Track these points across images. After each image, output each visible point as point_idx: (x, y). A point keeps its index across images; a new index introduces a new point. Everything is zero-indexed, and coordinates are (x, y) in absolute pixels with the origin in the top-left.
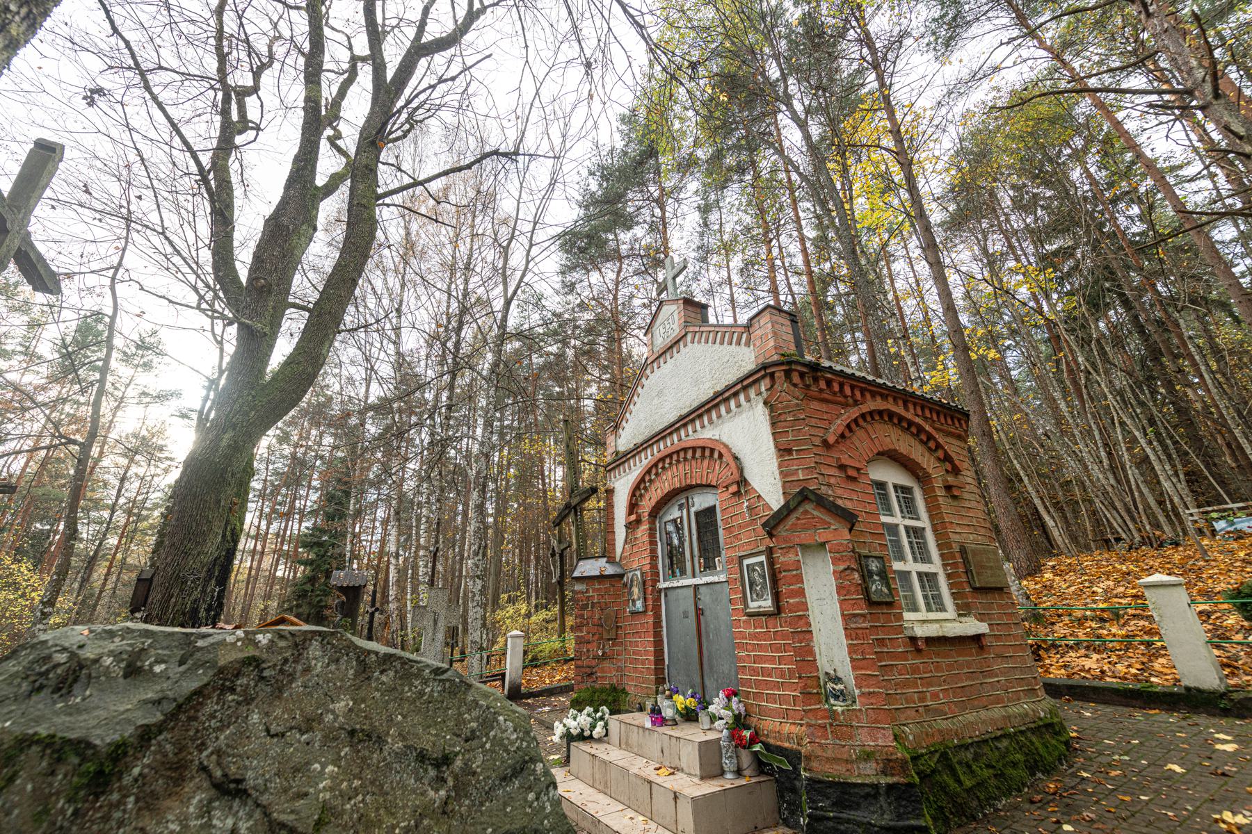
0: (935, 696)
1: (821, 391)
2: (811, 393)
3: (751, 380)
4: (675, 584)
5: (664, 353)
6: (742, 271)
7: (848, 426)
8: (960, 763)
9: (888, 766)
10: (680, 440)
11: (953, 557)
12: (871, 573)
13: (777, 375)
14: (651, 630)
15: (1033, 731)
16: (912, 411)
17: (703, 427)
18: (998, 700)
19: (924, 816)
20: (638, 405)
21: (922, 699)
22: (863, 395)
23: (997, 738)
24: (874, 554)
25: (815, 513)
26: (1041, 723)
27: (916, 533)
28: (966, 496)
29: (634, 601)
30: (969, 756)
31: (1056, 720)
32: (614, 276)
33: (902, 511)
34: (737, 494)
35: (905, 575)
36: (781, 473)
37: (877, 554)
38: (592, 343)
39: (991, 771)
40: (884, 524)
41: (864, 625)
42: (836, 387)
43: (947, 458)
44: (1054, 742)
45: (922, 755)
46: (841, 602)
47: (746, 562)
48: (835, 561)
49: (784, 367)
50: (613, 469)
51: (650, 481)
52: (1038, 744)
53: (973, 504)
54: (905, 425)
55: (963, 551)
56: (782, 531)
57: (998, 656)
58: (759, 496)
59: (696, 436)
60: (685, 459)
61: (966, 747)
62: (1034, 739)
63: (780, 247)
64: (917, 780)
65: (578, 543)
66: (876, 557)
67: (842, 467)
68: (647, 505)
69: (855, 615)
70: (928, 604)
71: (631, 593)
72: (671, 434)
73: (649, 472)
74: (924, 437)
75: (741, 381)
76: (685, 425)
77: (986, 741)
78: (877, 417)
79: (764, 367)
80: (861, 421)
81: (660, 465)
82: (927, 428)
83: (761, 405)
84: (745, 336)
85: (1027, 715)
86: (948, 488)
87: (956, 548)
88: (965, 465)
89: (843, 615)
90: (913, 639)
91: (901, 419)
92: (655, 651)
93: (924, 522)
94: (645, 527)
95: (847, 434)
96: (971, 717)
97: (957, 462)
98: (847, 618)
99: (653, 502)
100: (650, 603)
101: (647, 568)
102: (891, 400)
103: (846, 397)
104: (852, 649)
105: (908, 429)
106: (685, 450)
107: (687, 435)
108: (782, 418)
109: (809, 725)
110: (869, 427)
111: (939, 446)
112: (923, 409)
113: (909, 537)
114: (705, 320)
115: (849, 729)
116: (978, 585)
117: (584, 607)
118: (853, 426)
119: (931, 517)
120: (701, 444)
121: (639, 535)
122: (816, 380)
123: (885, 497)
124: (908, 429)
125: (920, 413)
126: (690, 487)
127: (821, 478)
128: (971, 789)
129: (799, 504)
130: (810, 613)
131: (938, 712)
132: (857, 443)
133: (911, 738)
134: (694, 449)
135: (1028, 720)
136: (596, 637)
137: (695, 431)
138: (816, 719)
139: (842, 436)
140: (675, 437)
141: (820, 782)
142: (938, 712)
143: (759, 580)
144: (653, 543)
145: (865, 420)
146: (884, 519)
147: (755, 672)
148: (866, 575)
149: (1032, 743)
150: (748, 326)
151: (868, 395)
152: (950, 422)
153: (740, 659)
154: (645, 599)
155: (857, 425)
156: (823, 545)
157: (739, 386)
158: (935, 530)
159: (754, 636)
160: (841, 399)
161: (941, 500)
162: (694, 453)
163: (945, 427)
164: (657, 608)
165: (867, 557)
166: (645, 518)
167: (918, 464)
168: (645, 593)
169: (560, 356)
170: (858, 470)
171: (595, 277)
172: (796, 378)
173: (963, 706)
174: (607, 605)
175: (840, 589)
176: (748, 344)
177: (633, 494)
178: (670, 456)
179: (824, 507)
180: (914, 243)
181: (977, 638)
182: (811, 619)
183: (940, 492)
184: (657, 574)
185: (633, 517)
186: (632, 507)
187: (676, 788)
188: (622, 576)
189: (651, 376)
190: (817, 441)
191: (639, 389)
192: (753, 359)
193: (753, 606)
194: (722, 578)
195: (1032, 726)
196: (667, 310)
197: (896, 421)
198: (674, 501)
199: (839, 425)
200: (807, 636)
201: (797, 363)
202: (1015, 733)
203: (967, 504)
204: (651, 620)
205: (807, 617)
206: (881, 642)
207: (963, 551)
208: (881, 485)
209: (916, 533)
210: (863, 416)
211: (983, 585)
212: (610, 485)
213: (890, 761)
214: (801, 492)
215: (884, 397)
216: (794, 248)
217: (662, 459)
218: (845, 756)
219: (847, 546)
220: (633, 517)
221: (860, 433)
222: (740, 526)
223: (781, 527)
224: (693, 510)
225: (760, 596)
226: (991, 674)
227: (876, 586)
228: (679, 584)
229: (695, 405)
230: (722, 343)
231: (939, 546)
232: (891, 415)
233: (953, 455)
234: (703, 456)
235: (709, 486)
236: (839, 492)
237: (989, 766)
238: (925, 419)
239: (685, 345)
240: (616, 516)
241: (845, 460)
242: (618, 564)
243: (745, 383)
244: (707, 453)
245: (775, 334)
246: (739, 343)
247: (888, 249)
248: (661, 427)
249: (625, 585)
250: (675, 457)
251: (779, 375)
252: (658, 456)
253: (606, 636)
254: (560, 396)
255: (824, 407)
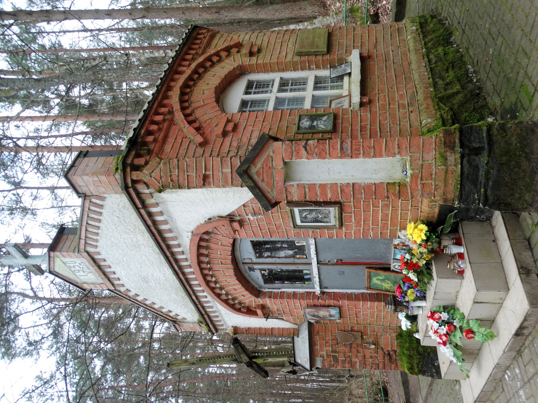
0: (401, 97)
1: (155, 140)
2: (156, 150)
3: (137, 201)
4: (317, 280)
5: (104, 274)
6: (43, 175)
7: (190, 123)
8: (446, 90)
9: (449, 145)
10: (190, 266)
11: (304, 62)
12: (312, 127)
13: (135, 178)
14: (354, 302)
15: (424, 37)
16: (184, 69)
17: (179, 246)
18: (405, 54)
19: (480, 126)
20: (155, 301)
21: (404, 107)
22: (164, 106)
23: (429, 61)
24: (297, 122)
25: (259, 165)
26: (420, 30)
27: (284, 85)
28: (259, 42)
29: (330, 316)
30: (440, 82)
31: (418, 20)
32: (28, 301)
33: (266, 92)
34: (241, 223)
35: (315, 99)
36: (224, 186)
37: (297, 119)
38: (98, 324)
39: (450, 70)
40: (275, 109)
41: (349, 143)
42: (154, 127)
43: (228, 49)
44: (432, 25)
45: (441, 115)
46: (331, 156)
47: (299, 222)
48: (299, 157)
49: (128, 169)
50: (214, 326)
51: (227, 294)
52: (433, 36)
53: (266, 39)
54: (196, 76)
55: (300, 54)
56: (273, 195)
57: (376, 47)
58: (244, 206)
59: (187, 251)
60: (208, 263)
61: (435, 85)
62: (430, 37)
63: (28, 138)
64: (456, 125)
65: (283, 356)
66: (300, 120)
67: (225, 134)
68: (249, 299)
69: (342, 148)
70: (337, 87)
71: (324, 318)
72: (184, 274)
73: (218, 296)
74: (208, 64)
75: (137, 209)
76: (176, 261)
77: (432, 70)
78: (186, 97)
79: (126, 188)
80: (188, 111)
81: (213, 285)
82: (201, 59)
83: (162, 194)
84: (94, 200)
85: (414, 38)
86: (251, 54)
87: (297, 59)
88: (236, 38)
89: (341, 157)
90: (362, 104)
91: (190, 78)
92: (371, 300)
93: (276, 77)
94: (268, 302)
95: (196, 125)
96: (416, 76)
97: (232, 43)
98: (343, 154)
99: (246, 293)
100: (332, 302)
101: (304, 303)
102: (173, 84)
103: (164, 120)
104: (366, 155)
105: (200, 75)
106: (199, 263)
107: (186, 260)
108: (175, 178)
109: (422, 195)
110: (194, 105)
111: (217, 54)
112: (185, 60)
113: (286, 91)
114: (74, 231)
115: (424, 167)
116: (325, 50)
117: (336, 359)
118: (191, 118)
119: (273, 71)
120: (195, 248)
121: (276, 308)
122: (145, 144)
123: (254, 103)
124: (200, 75)
125: (187, 63)
126: (235, 261)
127: (232, 154)
128: (462, 86)
129: (251, 178)
130: (339, 182)
131: (413, 97)
132: (206, 117)
133: (429, 120)
134: (199, 255)
135: (418, 38)
136: (360, 350)
137: (183, 253)
138: (418, 190)
139: (198, 129)
140: (187, 270)
141: (461, 195)
142: (413, 97)
143: (314, 215)
144: (282, 296)
145: (187, 108)
146: (271, 107)
147: (385, 226)
148: (313, 131)
149: (432, 39)
150: (83, 196)
151: (166, 102)
152: (199, 41)
153: (375, 235)
154: (329, 306)
155: (190, 115)
156: (285, 163)
157: (143, 211)
158: (283, 70)
159: (358, 223)
160: (166, 125)
161: (260, 61)
162: (203, 255)
163: (203, 46)
164: (337, 296)
165: (299, 128)
166: (260, 301)
167: (230, 72)
168: (324, 306)
169: (108, 358)
170: (228, 121)
171: (24, 321)
172: (140, 161)
173: (408, 79)
174: (335, 339)
175: (321, 156)
176: (103, 199)
177: (239, 311)
178: (204, 276)
179: (255, 158)
180: (43, 25)
181: (363, 59)
182: (344, 182)
183: (254, 60)
184: (308, 293)
185: (365, 100)
186: (250, 312)
187: (471, 302)
188: (310, 324)
189: (128, 286)
190: (200, 151)
191: (139, 299)
192: (118, 196)
193: (333, 221)
194: (312, 242)
195: (421, 37)
196: (59, 267)
197: (191, 83)
198: (246, 275)
199: (189, 131)
200: (357, 187)
201: (125, 158)
202: (426, 49)
203: (265, 43)
204: (346, 302)
205: (342, 186)
206: (363, 129)
207: (300, 54)
208: (244, 103)
209: (284, 85)
210: (183, 109)
211: (326, 46)
212: (230, 331)
213: (445, 143)
214: (241, 175)
215: (170, 88)
216: (30, 127)
217: (208, 283)
218: (443, 173)
219: (288, 145)
220: (259, 312)
221: (198, 114)
222: (269, 223)
223: (270, 196)
224: (255, 260)
225: (327, 216)
226: (387, 55)
227: (323, 124)
228: (317, 276)
229: (157, 250)
230: (99, 221)
231: (295, 70)
232: (186, 85)
233: (226, 45)
234: (207, 248)
235: (234, 245)
236: (245, 140)
237: (447, 70)
238: (193, 59)
239: (99, 254)
240: (258, 326)
241: (219, 130)
242: (300, 326)
243: (140, 206)
244: (203, 244)
245: (95, 174)
246: (101, 206)
247: (48, 47)
248: (177, 282)
249: (317, 322)
250: (206, 272)
251: (136, 175)
252: (204, 287)
253: (359, 341)
254: (149, 356)
255: (171, 140)
